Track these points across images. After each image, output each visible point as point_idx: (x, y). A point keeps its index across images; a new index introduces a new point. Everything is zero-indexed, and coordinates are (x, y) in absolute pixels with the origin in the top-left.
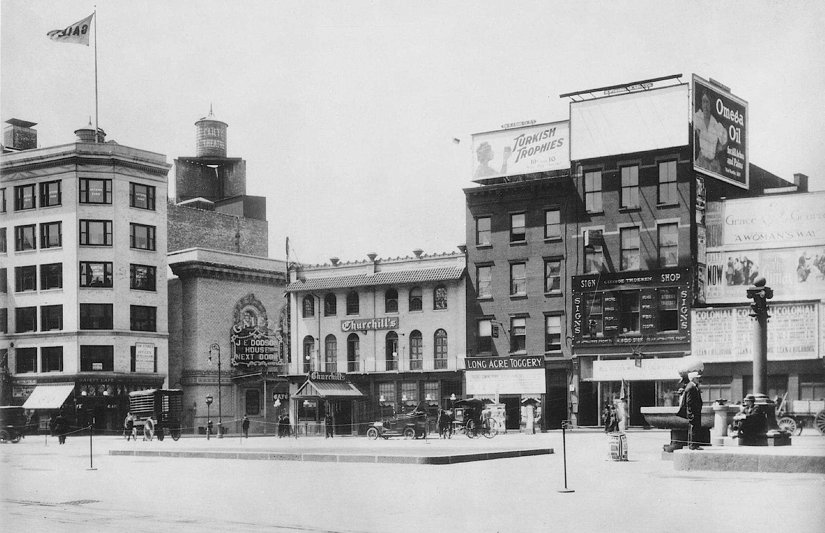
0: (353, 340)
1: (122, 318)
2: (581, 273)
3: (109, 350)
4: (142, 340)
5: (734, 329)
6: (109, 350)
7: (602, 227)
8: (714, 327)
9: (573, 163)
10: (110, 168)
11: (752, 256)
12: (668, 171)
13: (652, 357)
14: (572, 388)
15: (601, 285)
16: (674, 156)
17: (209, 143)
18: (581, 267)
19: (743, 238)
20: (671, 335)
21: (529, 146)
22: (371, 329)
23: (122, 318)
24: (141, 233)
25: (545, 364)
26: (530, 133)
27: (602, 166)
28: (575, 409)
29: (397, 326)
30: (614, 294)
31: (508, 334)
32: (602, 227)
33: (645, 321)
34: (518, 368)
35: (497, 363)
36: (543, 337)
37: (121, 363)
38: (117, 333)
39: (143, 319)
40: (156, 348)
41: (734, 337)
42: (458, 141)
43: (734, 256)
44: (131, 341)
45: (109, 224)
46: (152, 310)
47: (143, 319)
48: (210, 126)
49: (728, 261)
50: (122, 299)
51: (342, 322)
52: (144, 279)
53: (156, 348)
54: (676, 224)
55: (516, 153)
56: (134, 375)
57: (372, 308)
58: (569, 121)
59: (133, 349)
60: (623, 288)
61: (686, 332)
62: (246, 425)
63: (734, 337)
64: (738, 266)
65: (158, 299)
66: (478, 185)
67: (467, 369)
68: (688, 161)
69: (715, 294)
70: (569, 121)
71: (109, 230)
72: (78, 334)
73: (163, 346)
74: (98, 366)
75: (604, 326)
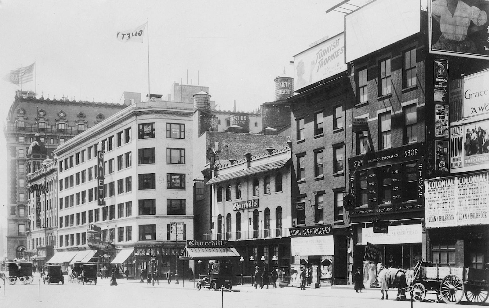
0: (239, 216)
1: (161, 207)
2: (354, 155)
3: (153, 227)
4: (175, 220)
5: (456, 196)
6: (153, 227)
7: (367, 115)
8: (441, 195)
9: (349, 64)
10: (154, 116)
11: (484, 126)
12: (411, 56)
13: (399, 224)
14: (349, 252)
15: (366, 164)
16: (412, 45)
17: (284, 91)
18: (354, 150)
19: (477, 110)
20: (412, 204)
21: (324, 57)
22: (246, 208)
23: (161, 207)
24: (176, 154)
25: (333, 232)
26: (324, 47)
27: (367, 64)
28: (351, 270)
29: (258, 206)
30: (375, 170)
31: (313, 207)
32: (367, 115)
33: (394, 193)
34: (318, 235)
35: (306, 231)
36: (332, 209)
37: (161, 235)
38: (157, 217)
39: (176, 208)
40: (185, 226)
41: (456, 203)
42: (293, 62)
43: (471, 127)
44: (168, 221)
45: (183, 151)
46: (182, 202)
47: (176, 208)
48: (281, 81)
49: (466, 133)
50: (161, 195)
51: (233, 204)
52: (176, 182)
53: (185, 226)
54: (414, 105)
55: (318, 64)
56: (169, 242)
57: (246, 191)
58: (344, 33)
59: (169, 226)
60: (379, 165)
61: (422, 201)
62: (118, 266)
63: (456, 203)
64: (474, 136)
65: (187, 195)
66: (298, 93)
67: (292, 236)
68: (423, 46)
69: (457, 164)
70: (344, 33)
71: (183, 155)
72: (137, 218)
73: (190, 224)
74: (148, 237)
75: (368, 198)
